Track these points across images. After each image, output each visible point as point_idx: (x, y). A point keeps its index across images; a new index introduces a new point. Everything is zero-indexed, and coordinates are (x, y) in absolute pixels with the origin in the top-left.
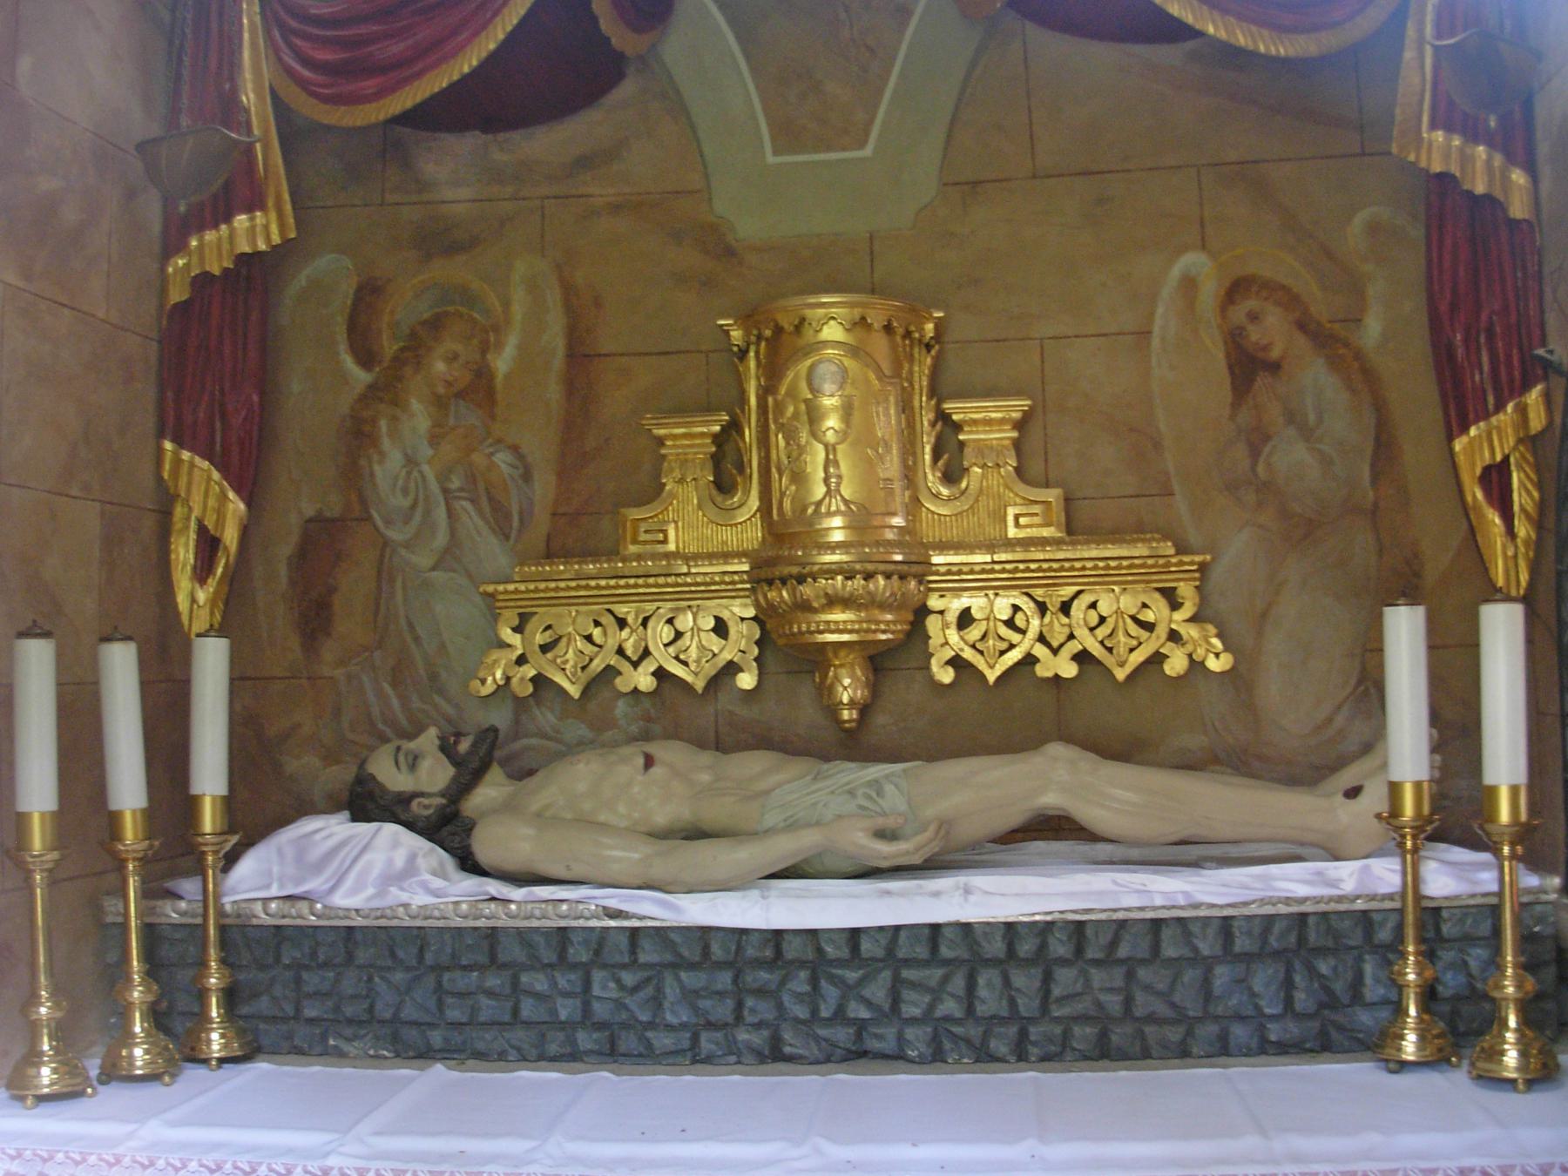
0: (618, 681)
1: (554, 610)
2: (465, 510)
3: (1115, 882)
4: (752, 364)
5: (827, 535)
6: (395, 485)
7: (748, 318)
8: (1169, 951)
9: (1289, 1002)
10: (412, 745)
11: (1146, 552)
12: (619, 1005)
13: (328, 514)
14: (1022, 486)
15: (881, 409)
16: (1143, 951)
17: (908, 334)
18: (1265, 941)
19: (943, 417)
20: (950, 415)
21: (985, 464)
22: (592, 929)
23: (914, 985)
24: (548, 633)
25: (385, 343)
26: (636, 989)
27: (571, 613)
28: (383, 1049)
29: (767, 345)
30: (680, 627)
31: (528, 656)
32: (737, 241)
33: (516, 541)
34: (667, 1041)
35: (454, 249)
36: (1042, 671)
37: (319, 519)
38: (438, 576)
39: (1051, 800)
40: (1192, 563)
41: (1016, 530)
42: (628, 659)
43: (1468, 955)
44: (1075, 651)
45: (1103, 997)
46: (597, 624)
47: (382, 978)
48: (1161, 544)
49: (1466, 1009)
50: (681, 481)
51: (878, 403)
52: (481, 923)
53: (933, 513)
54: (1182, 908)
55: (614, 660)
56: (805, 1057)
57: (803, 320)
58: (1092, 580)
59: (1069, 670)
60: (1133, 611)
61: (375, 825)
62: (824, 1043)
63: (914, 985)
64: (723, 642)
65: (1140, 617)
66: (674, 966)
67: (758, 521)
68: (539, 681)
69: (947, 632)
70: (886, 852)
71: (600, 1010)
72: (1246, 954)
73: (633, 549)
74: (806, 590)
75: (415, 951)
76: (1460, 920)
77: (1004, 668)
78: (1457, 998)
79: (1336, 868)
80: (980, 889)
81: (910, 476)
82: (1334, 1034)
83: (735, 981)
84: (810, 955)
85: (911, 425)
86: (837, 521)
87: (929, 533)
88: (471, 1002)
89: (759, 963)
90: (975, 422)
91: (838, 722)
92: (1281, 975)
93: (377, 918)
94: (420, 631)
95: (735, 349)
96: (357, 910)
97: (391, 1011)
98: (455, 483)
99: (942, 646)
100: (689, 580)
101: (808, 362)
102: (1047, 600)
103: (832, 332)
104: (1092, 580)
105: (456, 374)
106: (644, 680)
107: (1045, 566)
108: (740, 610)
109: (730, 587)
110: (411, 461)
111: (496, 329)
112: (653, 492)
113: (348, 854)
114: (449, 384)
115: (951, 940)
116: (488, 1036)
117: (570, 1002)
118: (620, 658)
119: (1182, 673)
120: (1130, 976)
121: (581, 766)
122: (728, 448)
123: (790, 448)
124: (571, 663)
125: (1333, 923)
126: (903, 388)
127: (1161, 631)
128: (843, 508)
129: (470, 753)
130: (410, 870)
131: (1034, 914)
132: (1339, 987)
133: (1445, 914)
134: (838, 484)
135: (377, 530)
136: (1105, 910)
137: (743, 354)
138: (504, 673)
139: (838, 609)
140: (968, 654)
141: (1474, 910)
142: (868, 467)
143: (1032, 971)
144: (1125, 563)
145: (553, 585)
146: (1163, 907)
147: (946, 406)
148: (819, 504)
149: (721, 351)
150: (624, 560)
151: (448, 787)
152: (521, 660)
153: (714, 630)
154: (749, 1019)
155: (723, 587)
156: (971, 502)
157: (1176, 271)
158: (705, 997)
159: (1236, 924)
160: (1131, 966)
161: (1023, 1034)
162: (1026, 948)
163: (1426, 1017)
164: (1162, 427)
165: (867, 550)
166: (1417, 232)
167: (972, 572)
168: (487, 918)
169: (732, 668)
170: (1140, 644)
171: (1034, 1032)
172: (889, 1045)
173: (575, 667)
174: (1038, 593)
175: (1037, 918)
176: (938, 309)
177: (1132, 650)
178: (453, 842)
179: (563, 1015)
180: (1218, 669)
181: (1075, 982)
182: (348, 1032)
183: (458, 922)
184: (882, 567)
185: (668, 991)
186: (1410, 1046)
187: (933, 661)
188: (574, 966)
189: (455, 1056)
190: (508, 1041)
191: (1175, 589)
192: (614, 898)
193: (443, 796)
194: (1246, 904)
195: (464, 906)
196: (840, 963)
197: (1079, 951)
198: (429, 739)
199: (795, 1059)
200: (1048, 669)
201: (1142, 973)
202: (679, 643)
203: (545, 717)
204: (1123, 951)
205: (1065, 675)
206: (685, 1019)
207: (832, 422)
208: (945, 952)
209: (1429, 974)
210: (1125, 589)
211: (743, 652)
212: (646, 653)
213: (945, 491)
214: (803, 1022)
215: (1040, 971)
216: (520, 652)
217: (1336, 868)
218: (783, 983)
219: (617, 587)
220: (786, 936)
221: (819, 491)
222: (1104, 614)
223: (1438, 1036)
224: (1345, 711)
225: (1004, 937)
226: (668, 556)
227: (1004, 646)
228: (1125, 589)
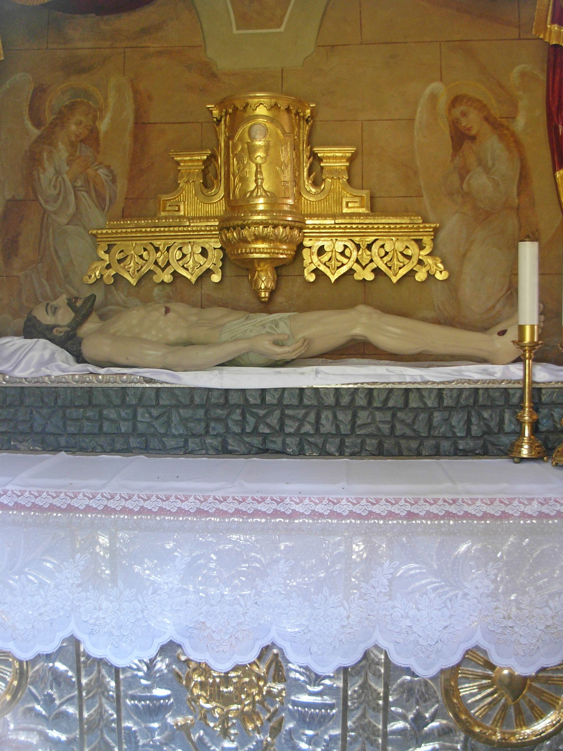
0: (154, 277)
1: (125, 243)
2: (84, 197)
3: (388, 370)
4: (223, 127)
5: (256, 207)
6: (50, 184)
7: (221, 104)
8: (413, 404)
9: (469, 430)
10: (55, 303)
11: (408, 221)
12: (150, 425)
13: (17, 198)
14: (352, 189)
15: (283, 148)
16: (400, 404)
17: (297, 114)
18: (458, 402)
19: (313, 155)
20: (317, 154)
21: (333, 178)
22: (138, 388)
23: (291, 417)
24: (121, 254)
25: (47, 117)
26: (158, 417)
27: (132, 244)
28: (37, 446)
29: (230, 116)
30: (185, 252)
31: (112, 265)
32: (218, 70)
33: (108, 211)
34: (172, 443)
35: (82, 71)
36: (357, 277)
37: (13, 200)
38: (70, 228)
39: (358, 331)
40: (430, 227)
41: (346, 209)
42: (160, 267)
43: (554, 411)
44: (373, 268)
45: (381, 426)
46: (145, 250)
47: (37, 412)
48: (416, 218)
49: (552, 437)
50: (187, 182)
51: (282, 145)
52: (85, 385)
53: (307, 200)
54: (419, 383)
55: (152, 267)
56: (238, 451)
57: (247, 104)
58: (382, 234)
59: (370, 277)
60: (401, 250)
61: (35, 340)
62: (248, 445)
63: (291, 417)
64: (205, 259)
65: (404, 252)
66: (176, 406)
67: (223, 202)
68: (117, 277)
69: (312, 257)
70: (280, 352)
71: (141, 428)
72: (449, 407)
73: (163, 214)
74: (245, 232)
75: (53, 399)
76: (550, 395)
77: (339, 275)
78: (548, 431)
79: (493, 368)
80: (323, 372)
81: (297, 181)
82: (490, 447)
83: (206, 414)
84: (242, 402)
85: (298, 157)
86: (261, 200)
87: (305, 209)
88: (79, 424)
89: (218, 406)
90: (329, 157)
91: (259, 298)
92: (466, 418)
93: (35, 383)
94: (60, 253)
95: (215, 120)
96: (25, 379)
97: (41, 428)
98: (79, 183)
99: (310, 263)
100: (189, 229)
101: (250, 124)
102: (361, 243)
103: (262, 111)
104: (382, 234)
105: (81, 131)
106: (167, 277)
107: (360, 226)
108: (214, 244)
109: (209, 233)
110: (58, 173)
111: (101, 110)
112: (174, 187)
113: (23, 352)
114: (77, 136)
115: (309, 396)
116: (87, 440)
117: (126, 423)
118: (156, 266)
119: (424, 280)
120: (394, 416)
121: (135, 312)
122: (211, 169)
123: (239, 166)
124: (132, 268)
125: (491, 393)
126: (295, 139)
127: (415, 260)
128: (264, 194)
129: (82, 306)
130: (52, 359)
131: (349, 384)
132: (492, 424)
133: (544, 391)
134: (262, 183)
135: (41, 205)
136: (382, 383)
137: (219, 121)
138: (100, 273)
139: (260, 242)
140: (322, 268)
141: (557, 390)
142: (277, 176)
143: (348, 412)
144: (398, 226)
145: (124, 230)
146: (410, 383)
147: (315, 149)
148: (252, 192)
149: (209, 122)
150: (159, 219)
151: (71, 322)
152: (108, 267)
153: (201, 253)
154: (212, 432)
155: (206, 233)
156: (326, 195)
157: (427, 91)
158: (191, 422)
159: (445, 392)
160: (394, 411)
161: (342, 443)
162: (345, 400)
163: (532, 437)
164: (418, 164)
165: (275, 214)
166: (543, 77)
167: (325, 228)
168: (88, 382)
169: (209, 272)
170: (404, 265)
171: (348, 442)
172: (278, 446)
173: (134, 270)
174: (357, 239)
175: (350, 386)
176: (313, 103)
177: (400, 268)
178: (72, 347)
179: (123, 430)
180: (441, 279)
181: (368, 418)
182: (21, 438)
183: (74, 384)
184: (282, 222)
185: (173, 418)
186: (525, 452)
187: (305, 271)
188: (129, 406)
189: (71, 450)
190: (96, 443)
191: (422, 240)
192: (148, 373)
193: (69, 327)
194: (450, 382)
195: (77, 377)
196: (255, 406)
197: (370, 403)
198: (62, 300)
199: (234, 452)
200: (360, 276)
201: (399, 414)
202: (184, 259)
203: (120, 296)
204: (391, 404)
205: (368, 279)
206: (181, 432)
207: (260, 154)
208: (306, 402)
209: (535, 417)
210: (398, 239)
211: (215, 264)
212: (168, 264)
213: (313, 190)
214: (238, 434)
215: (351, 412)
216: (108, 263)
217: (493, 368)
218: (228, 415)
219: (155, 232)
220: (230, 392)
221: (253, 186)
222: (387, 251)
223: (538, 446)
224: (501, 302)
225: (334, 395)
226: (180, 217)
227: (340, 264)
228: (398, 239)
